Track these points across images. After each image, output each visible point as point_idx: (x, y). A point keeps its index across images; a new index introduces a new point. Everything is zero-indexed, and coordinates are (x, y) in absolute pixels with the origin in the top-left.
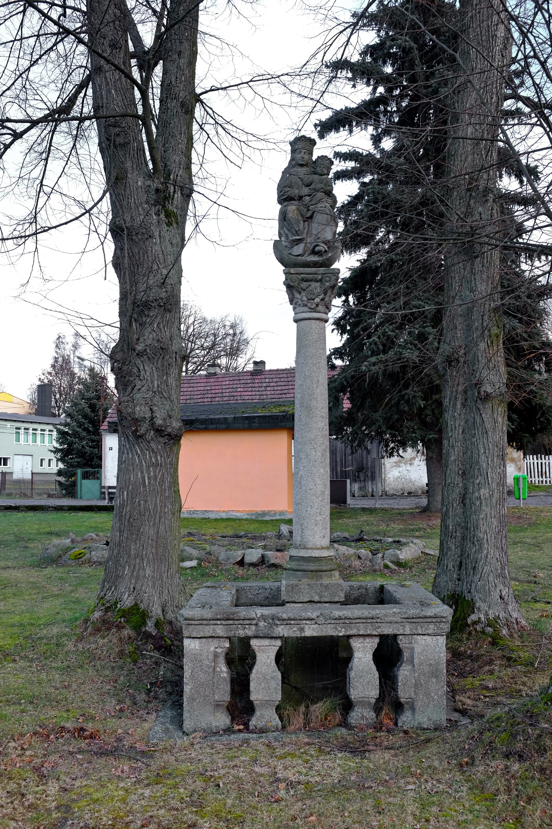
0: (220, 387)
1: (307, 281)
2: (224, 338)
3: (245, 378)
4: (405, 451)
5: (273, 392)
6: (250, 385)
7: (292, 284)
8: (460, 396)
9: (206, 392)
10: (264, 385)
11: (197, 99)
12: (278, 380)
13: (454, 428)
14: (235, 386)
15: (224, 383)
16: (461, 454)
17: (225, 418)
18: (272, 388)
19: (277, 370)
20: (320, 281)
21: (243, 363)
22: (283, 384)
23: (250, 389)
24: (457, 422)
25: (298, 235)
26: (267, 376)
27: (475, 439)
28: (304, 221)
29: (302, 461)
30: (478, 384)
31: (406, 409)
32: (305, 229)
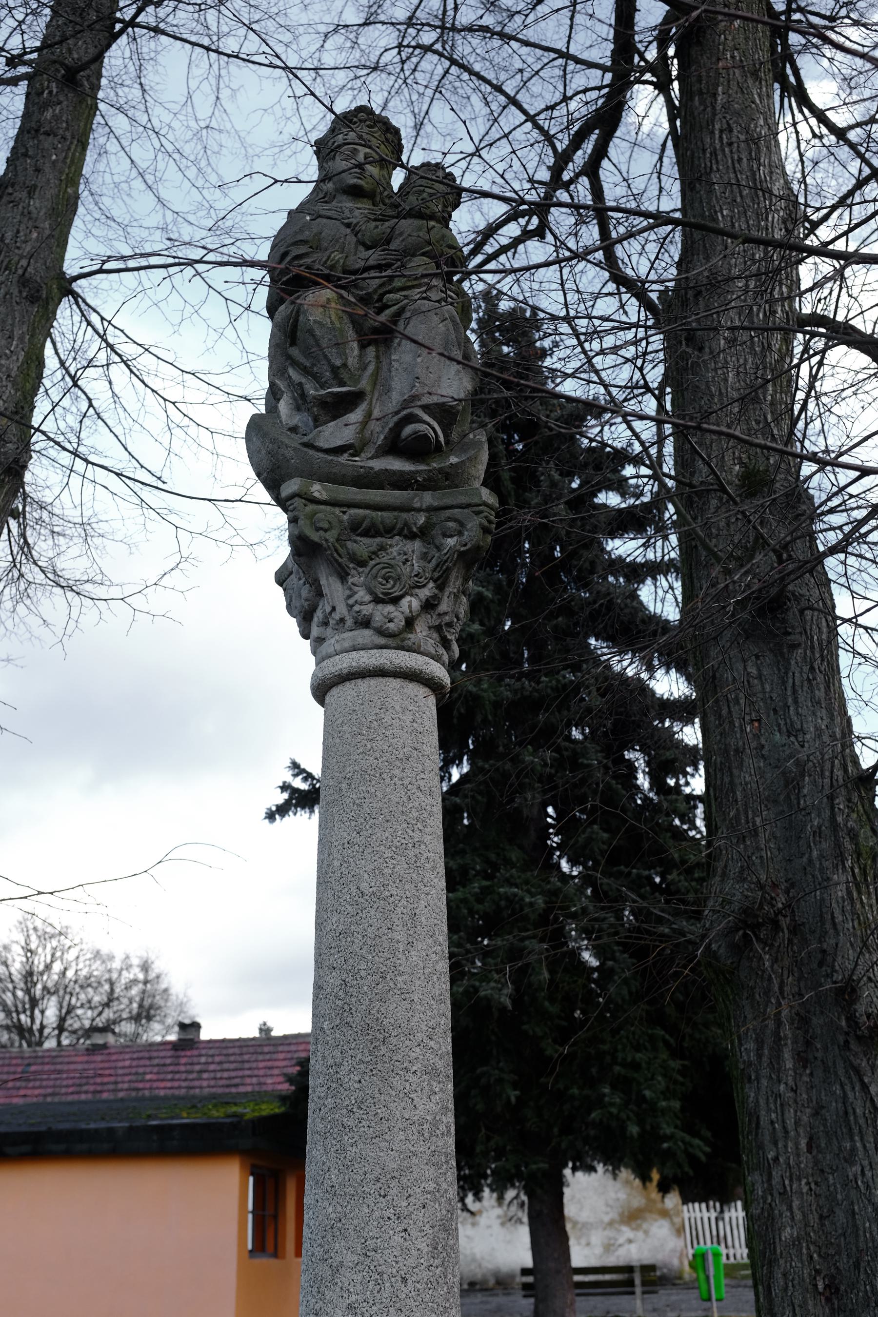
0: (112, 1072)
1: (371, 531)
2: (127, 988)
3: (162, 1054)
4: (478, 1198)
5: (212, 1083)
6: (171, 1068)
7: (315, 537)
8: (787, 1030)
9: (84, 1081)
10: (197, 1068)
11: (65, 287)
12: (222, 1058)
13: (780, 1134)
14: (141, 1070)
15: (120, 1064)
16: (813, 1219)
17: (111, 1131)
18: (212, 1075)
19: (224, 1041)
20: (423, 534)
21: (161, 1033)
22: (232, 1066)
23: (169, 1076)
24: (790, 1114)
25: (342, 384)
26: (203, 1052)
27: (857, 1169)
28: (363, 347)
29: (345, 1277)
30: (848, 992)
31: (480, 1107)
32: (364, 368)
